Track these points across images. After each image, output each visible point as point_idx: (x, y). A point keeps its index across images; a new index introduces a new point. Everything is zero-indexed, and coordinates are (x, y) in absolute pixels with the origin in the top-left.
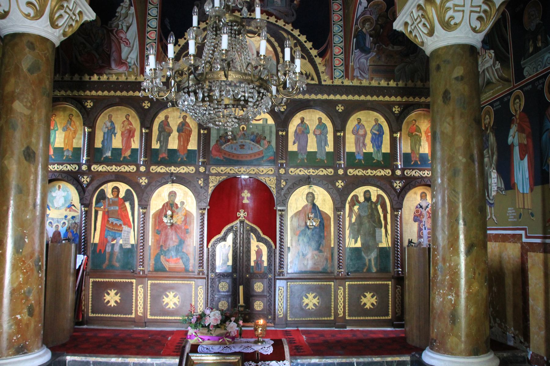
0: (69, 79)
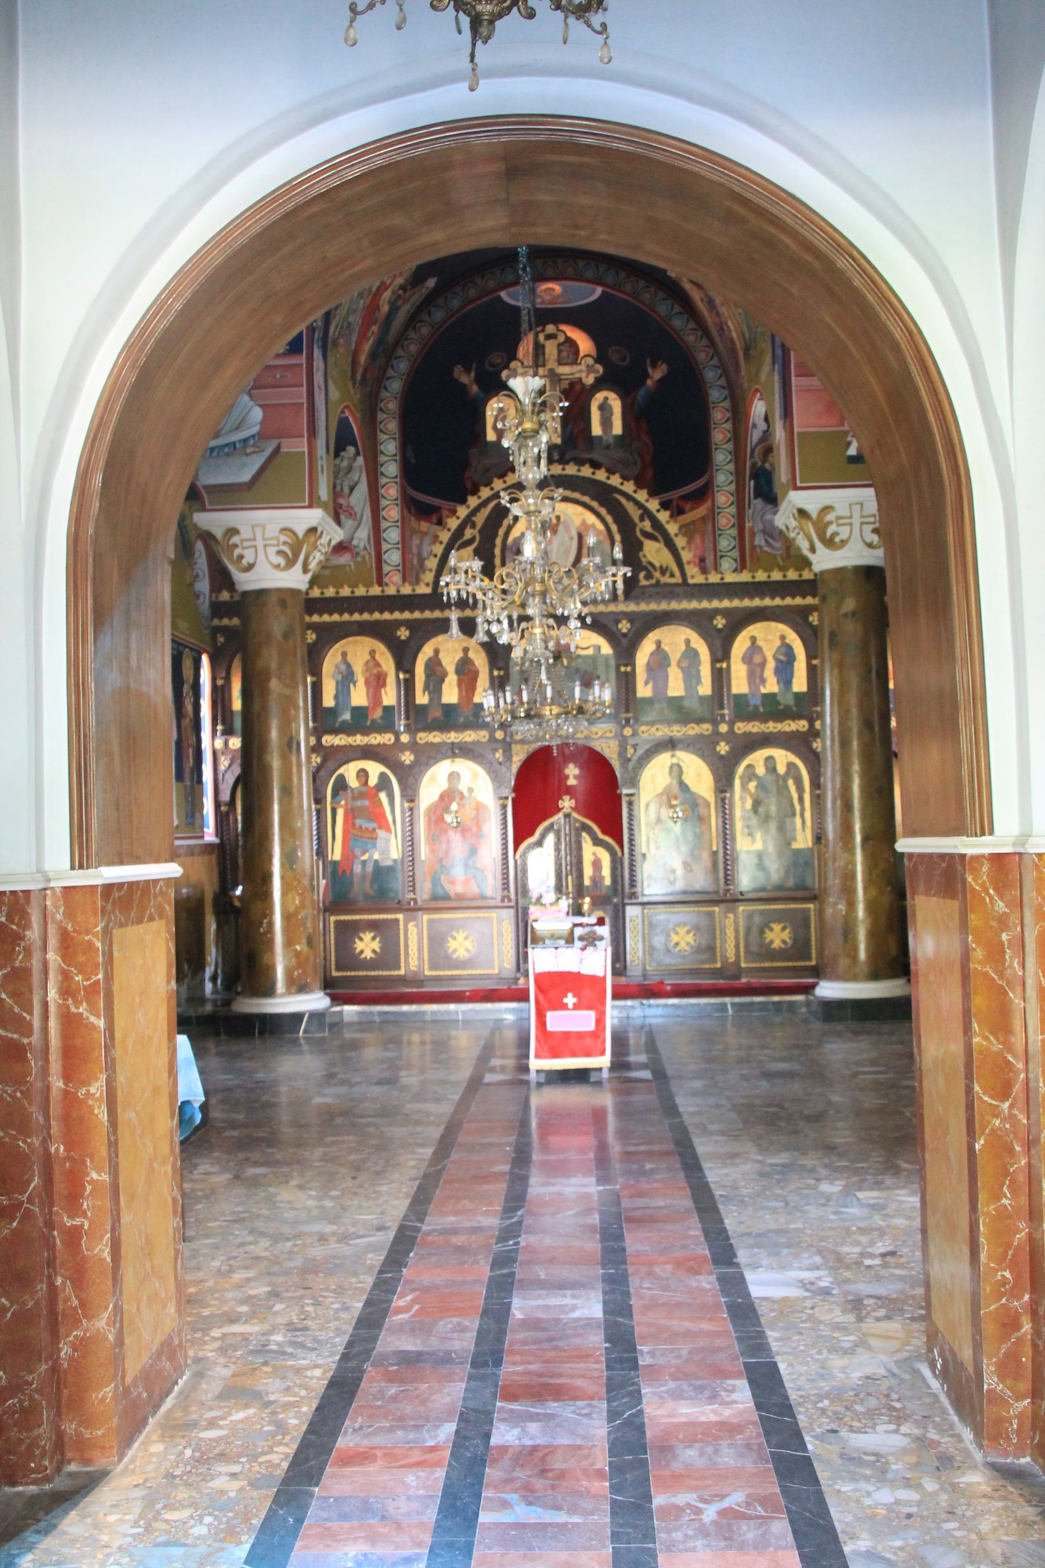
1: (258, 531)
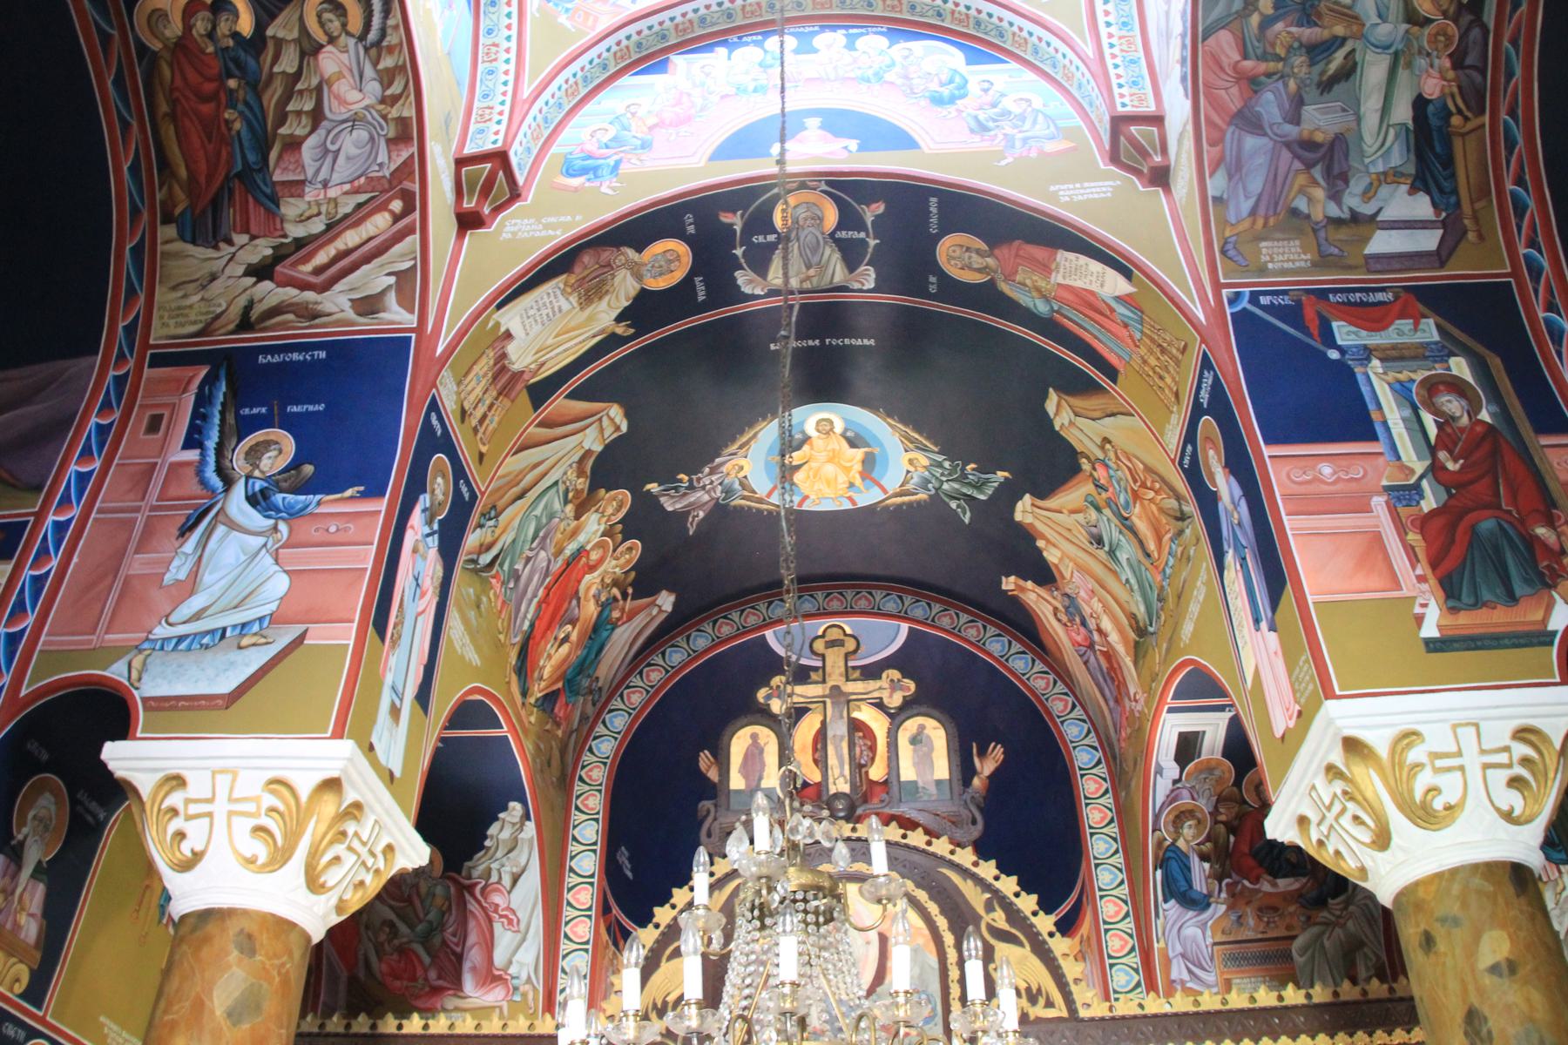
0: (341, 1030)
1: (223, 781)
